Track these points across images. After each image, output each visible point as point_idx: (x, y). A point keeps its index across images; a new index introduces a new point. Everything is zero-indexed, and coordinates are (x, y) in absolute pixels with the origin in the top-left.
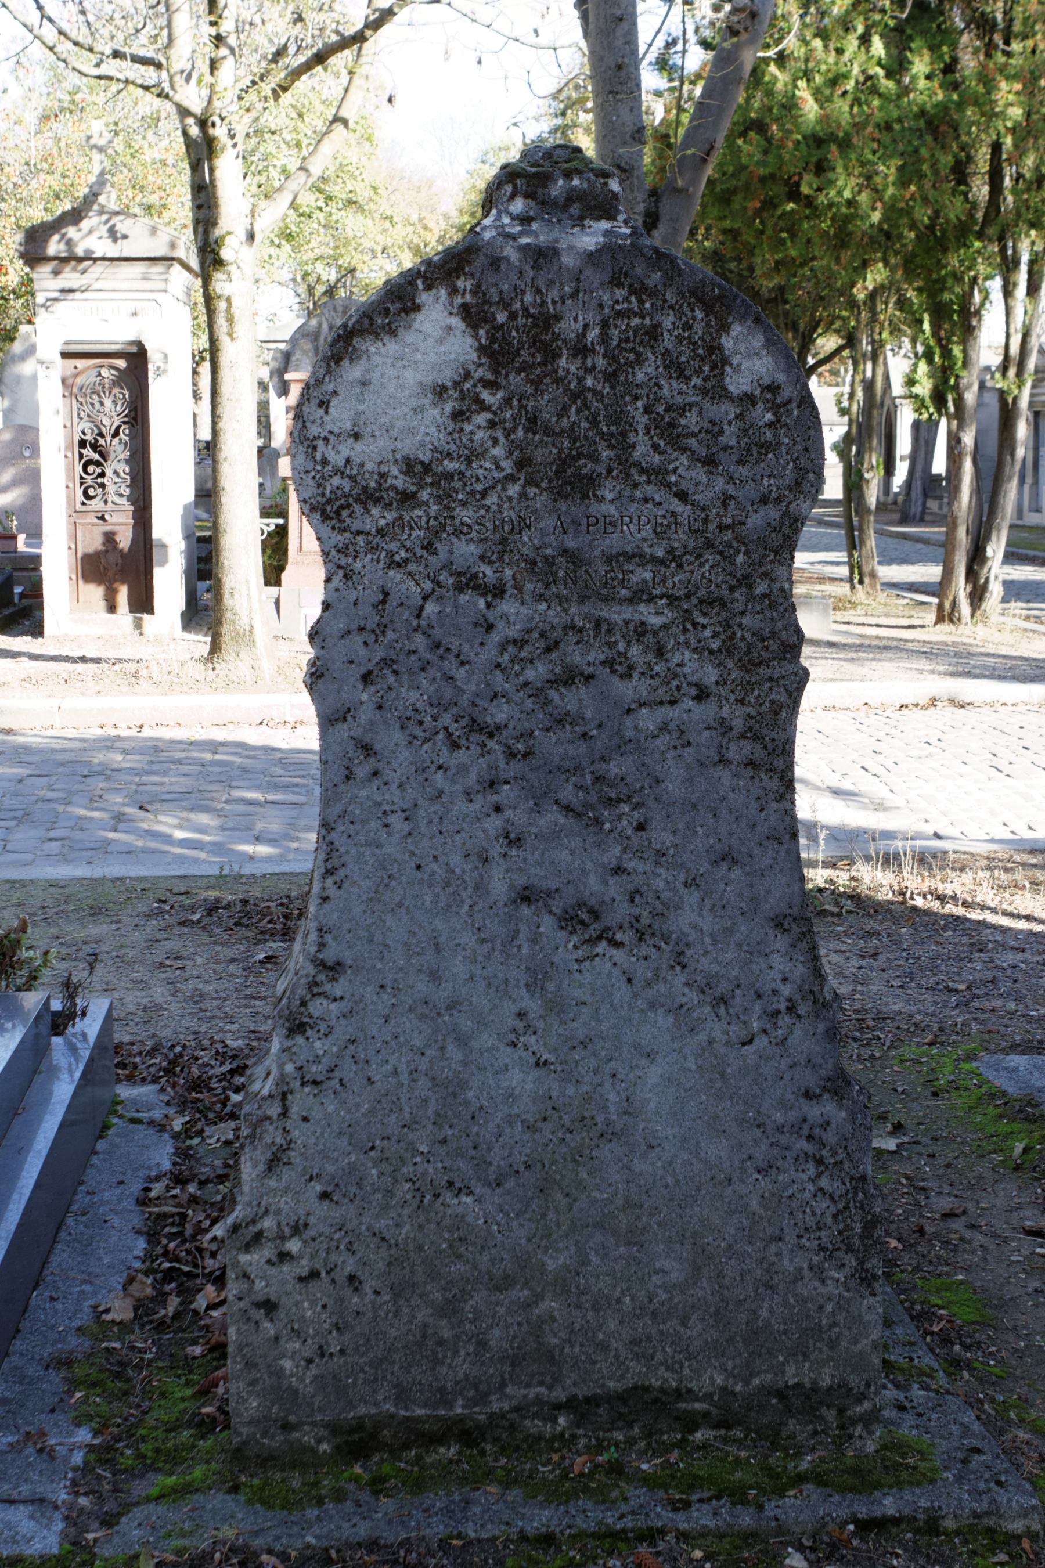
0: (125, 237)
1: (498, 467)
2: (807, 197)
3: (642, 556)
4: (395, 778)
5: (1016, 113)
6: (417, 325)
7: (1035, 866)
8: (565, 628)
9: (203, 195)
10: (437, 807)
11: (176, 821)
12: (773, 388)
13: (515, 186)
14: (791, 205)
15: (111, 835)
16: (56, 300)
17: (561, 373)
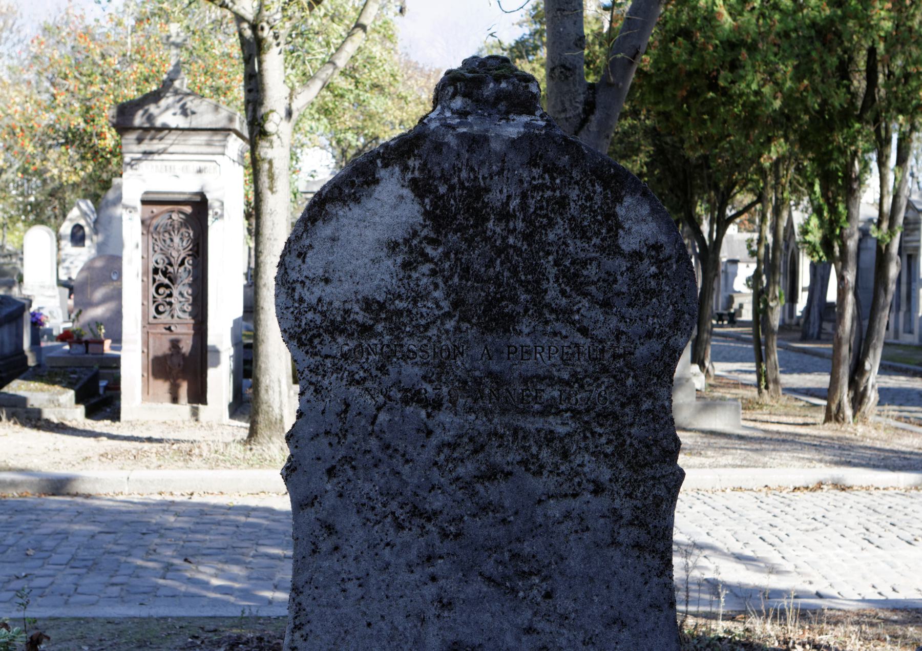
0: (193, 113)
1: (438, 306)
2: (723, 88)
3: (551, 378)
4: (352, 552)
5: (888, 25)
6: (376, 195)
7: (895, 622)
8: (489, 435)
9: (253, 81)
10: (385, 576)
11: (213, 571)
12: (657, 247)
13: (456, 88)
14: (711, 94)
15: (161, 581)
16: (139, 160)
17: (489, 233)
